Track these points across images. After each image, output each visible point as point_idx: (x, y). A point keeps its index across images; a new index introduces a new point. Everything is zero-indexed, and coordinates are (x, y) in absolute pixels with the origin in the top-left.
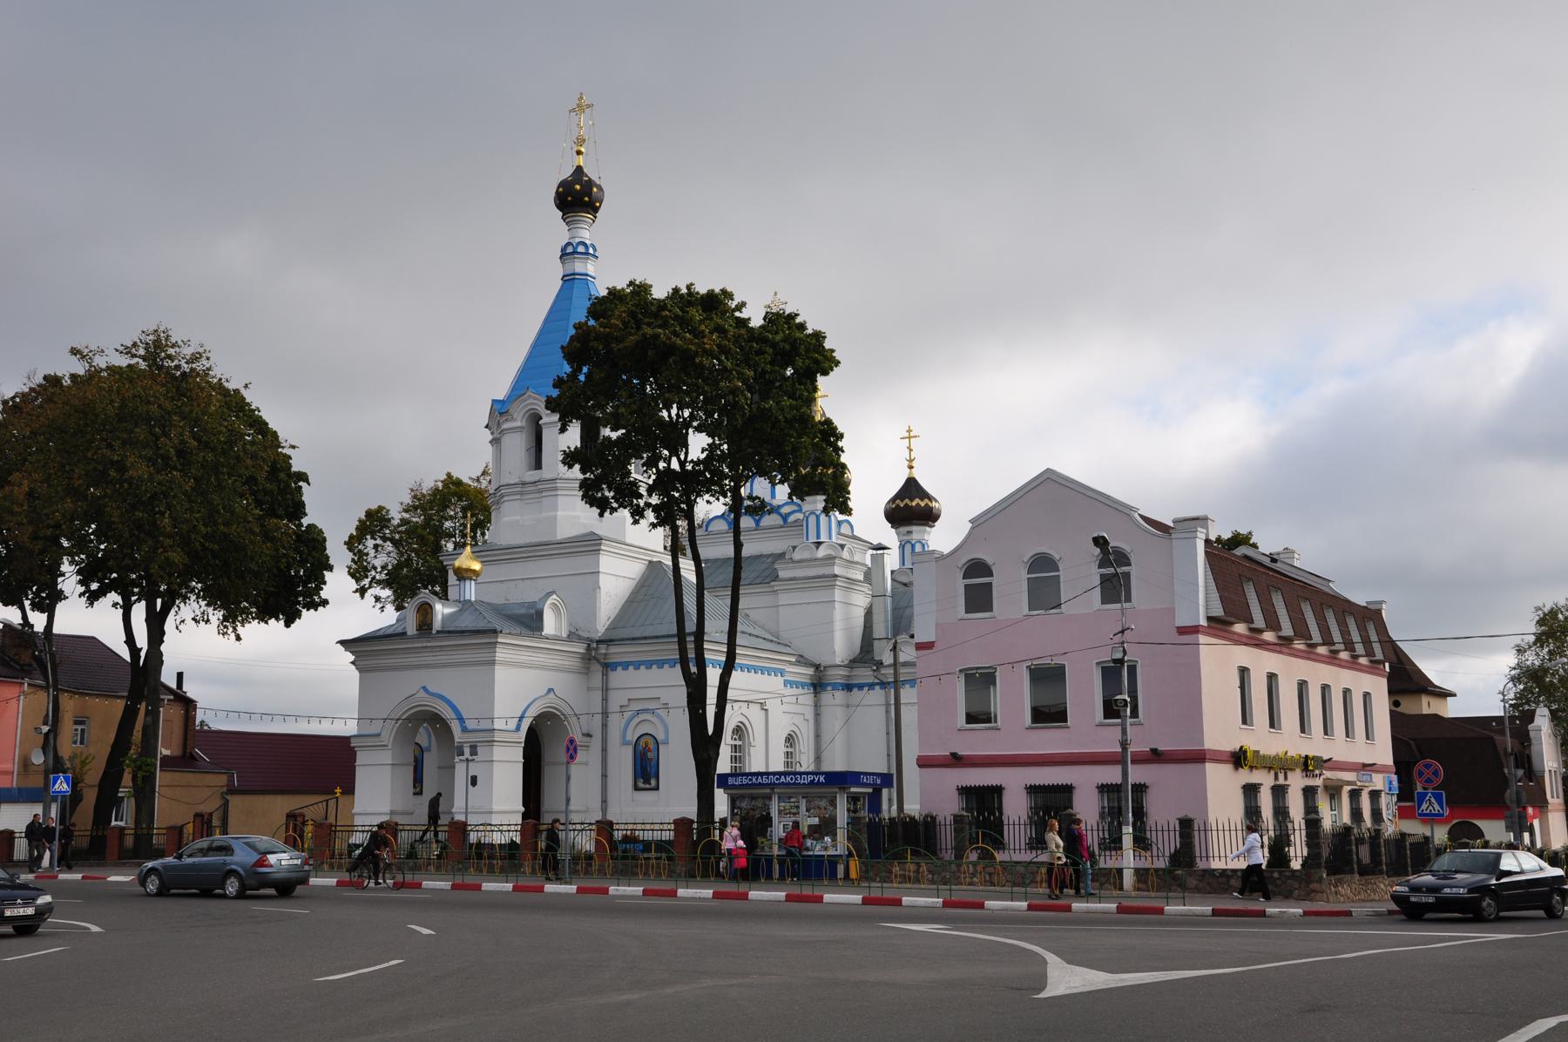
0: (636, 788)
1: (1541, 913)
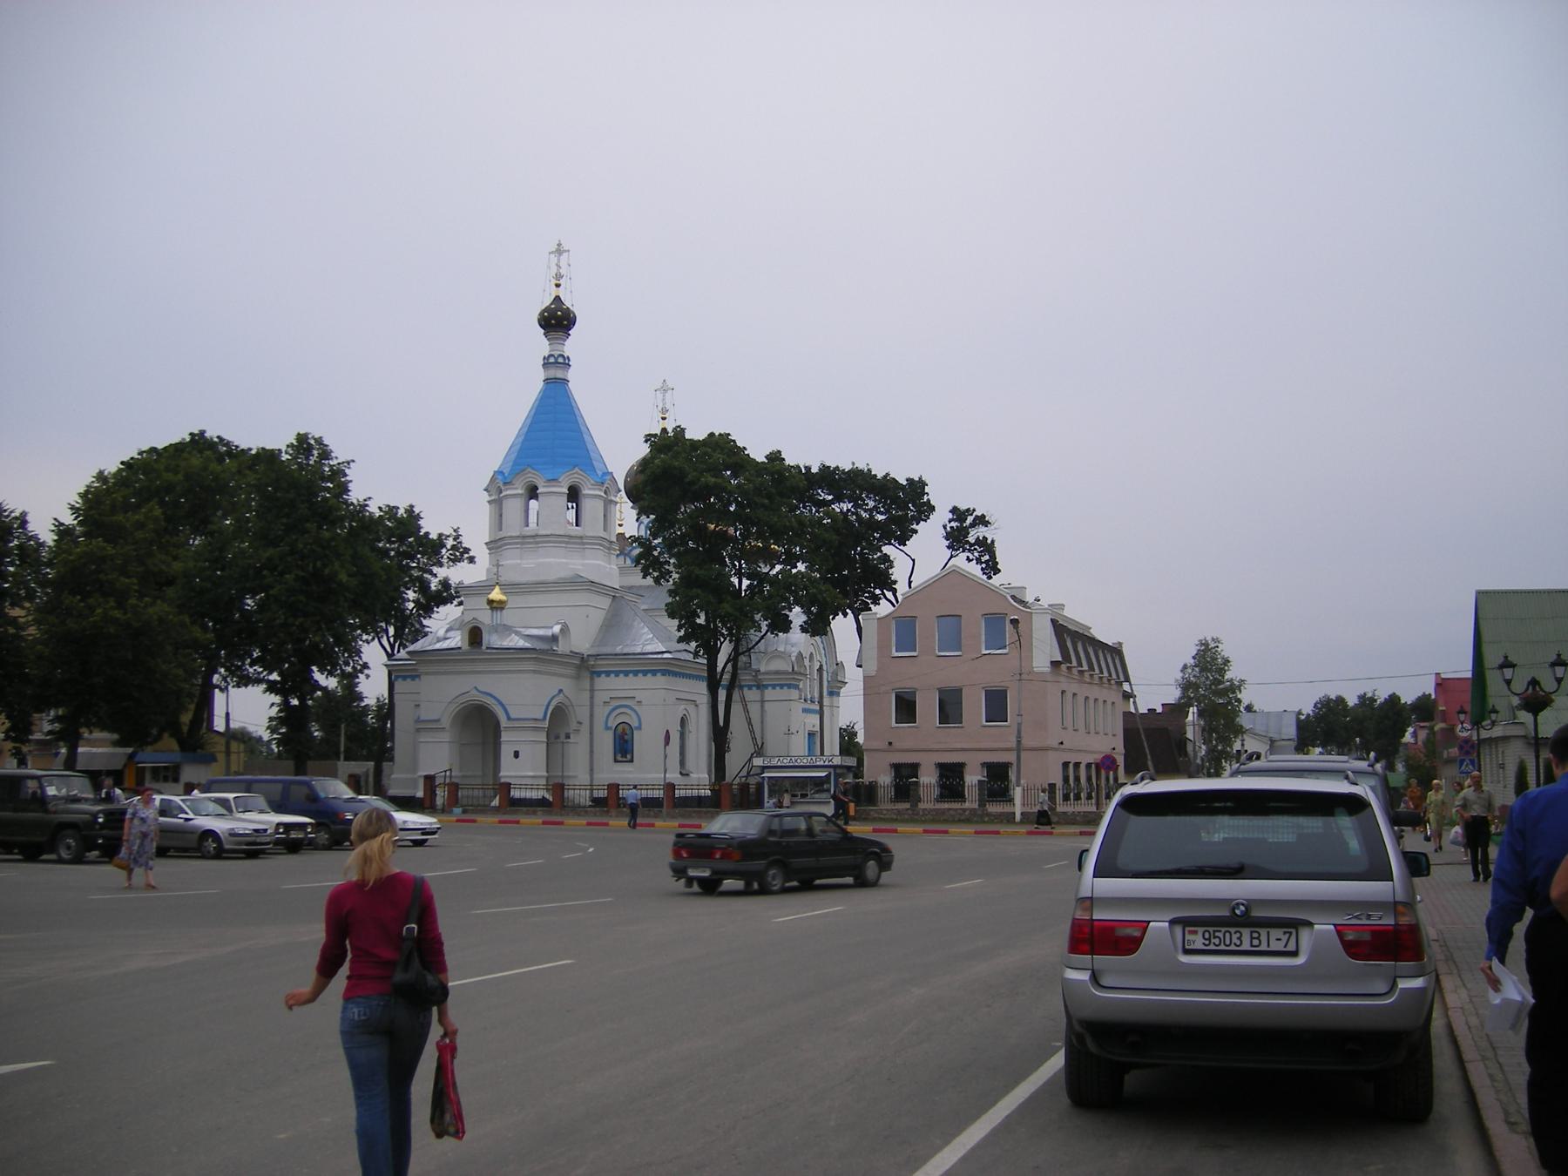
0: (616, 761)
1: (849, 880)
